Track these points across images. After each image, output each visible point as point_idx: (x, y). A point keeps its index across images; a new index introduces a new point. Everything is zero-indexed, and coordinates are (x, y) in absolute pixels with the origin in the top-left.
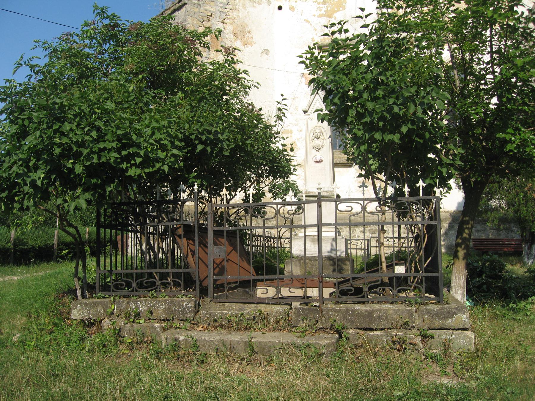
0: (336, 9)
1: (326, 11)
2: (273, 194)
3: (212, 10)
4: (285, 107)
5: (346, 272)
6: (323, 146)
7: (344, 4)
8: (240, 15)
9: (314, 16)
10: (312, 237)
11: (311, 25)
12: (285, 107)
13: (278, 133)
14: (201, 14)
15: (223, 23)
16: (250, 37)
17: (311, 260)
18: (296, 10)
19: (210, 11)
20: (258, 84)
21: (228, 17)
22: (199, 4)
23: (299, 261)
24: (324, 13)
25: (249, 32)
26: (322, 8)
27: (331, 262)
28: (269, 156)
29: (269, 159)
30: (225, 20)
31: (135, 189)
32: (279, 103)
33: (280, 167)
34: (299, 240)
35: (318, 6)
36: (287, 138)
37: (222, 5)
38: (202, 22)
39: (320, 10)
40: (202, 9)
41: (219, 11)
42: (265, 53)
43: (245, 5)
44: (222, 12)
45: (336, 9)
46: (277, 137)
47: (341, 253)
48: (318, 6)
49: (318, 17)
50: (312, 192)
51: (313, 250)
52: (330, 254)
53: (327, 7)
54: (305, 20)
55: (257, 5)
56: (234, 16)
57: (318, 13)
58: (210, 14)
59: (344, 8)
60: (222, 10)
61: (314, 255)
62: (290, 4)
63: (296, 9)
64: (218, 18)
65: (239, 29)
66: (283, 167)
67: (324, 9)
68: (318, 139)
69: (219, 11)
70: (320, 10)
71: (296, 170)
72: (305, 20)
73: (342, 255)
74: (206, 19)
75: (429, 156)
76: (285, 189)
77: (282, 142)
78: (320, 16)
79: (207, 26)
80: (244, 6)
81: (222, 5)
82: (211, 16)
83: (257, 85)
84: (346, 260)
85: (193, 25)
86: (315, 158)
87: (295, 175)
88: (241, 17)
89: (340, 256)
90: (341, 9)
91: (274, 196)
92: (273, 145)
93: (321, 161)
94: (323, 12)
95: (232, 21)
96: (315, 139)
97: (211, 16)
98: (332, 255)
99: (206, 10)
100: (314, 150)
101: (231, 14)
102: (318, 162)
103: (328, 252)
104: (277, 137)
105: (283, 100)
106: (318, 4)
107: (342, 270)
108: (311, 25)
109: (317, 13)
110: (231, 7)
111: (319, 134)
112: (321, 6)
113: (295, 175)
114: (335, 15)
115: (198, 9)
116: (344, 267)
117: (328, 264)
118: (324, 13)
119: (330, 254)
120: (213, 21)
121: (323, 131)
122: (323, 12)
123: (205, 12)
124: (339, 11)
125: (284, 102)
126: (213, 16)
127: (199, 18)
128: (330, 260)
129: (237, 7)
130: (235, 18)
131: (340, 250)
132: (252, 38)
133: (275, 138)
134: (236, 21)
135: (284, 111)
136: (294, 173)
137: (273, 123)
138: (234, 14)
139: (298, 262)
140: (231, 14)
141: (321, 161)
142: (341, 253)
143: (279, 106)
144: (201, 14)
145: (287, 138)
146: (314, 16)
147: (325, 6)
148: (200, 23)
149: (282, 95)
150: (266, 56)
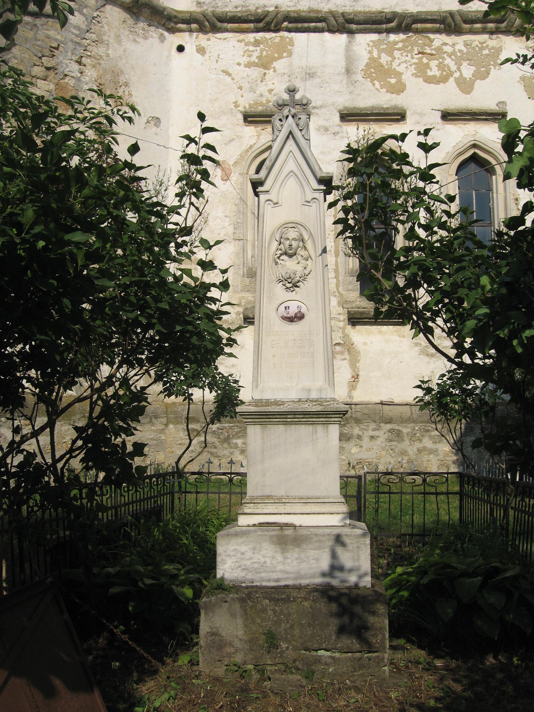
0: (276, 55)
1: (259, 58)
2: (165, 383)
3: (59, 37)
4: (210, 153)
5: (376, 635)
6: (304, 277)
7: (289, 47)
8: (110, 52)
9: (239, 64)
10: (274, 532)
11: (233, 79)
12: (210, 153)
13: (187, 231)
14: (39, 43)
15: (79, 63)
16: (127, 93)
17: (276, 601)
18: (208, 55)
19: (56, 40)
20: (133, 109)
21: (89, 54)
22: (35, 25)
23: (242, 600)
24: (256, 61)
25: (126, 84)
26: (253, 51)
27: (334, 607)
28: (157, 299)
29: (158, 309)
30: (83, 59)
31: (415, 254)
32: (191, 140)
33: (192, 334)
34: (240, 540)
35: (246, 48)
36: (218, 242)
37: (77, 32)
38: (40, 58)
39: (250, 56)
40: (41, 34)
41: (72, 41)
42: (152, 123)
43: (119, 36)
44: (78, 43)
45: (276, 55)
46: (185, 243)
47: (361, 577)
48: (246, 48)
49: (246, 66)
50: (276, 403)
51: (280, 567)
52: (327, 580)
53: (262, 51)
54: (223, 71)
55: (140, 40)
56: (100, 53)
57: (245, 60)
58: (55, 45)
59: (290, 54)
60: (78, 40)
61: (282, 583)
62: (198, 43)
63: (208, 52)
64: (70, 54)
65: (108, 77)
66: (200, 335)
67: (256, 54)
68: (291, 256)
69: (72, 41)
70: (250, 56)
71: (235, 341)
72: (223, 71)
73: (362, 584)
74: (47, 53)
75: (84, 306)
76: (190, 374)
77: (201, 254)
78: (249, 65)
79: (49, 65)
80: (118, 37)
81: (77, 32)
82: (57, 49)
83: (130, 114)
84: (377, 600)
85: (22, 61)
86: (282, 308)
87: (231, 355)
88: (111, 56)
89: (356, 586)
90: (285, 55)
91: (165, 390)
92: (172, 267)
93: (299, 317)
94: (254, 59)
95: (95, 61)
96: (284, 257)
97: (57, 49)
98: (335, 582)
99: (48, 37)
100: (279, 288)
101: (94, 50)
102: (290, 320)
103: (324, 575)
104: (185, 243)
105: (206, 130)
106: (246, 44)
107: (366, 628)
108: (233, 79)
109: (245, 60)
110: (94, 36)
111: (294, 244)
112: (251, 48)
113: (231, 355)
114: (275, 64)
115: (32, 33)
116: (372, 620)
117: (324, 610)
118: (256, 61)
119: (327, 580)
120: (61, 58)
121: (306, 237)
122: (254, 59)
123: (46, 40)
124: (280, 57)
125: (208, 138)
126: (61, 49)
127: (33, 50)
128: (331, 599)
129: (105, 38)
130: (101, 57)
131: (358, 569)
132: (130, 95)
133: (178, 246)
134: (102, 62)
135: (207, 164)
136: (227, 350)
137: (171, 200)
138: (101, 50)
139: (237, 606)
140: (94, 50)
141: (299, 317)
142: (361, 577)
143: (192, 149)
144: (39, 43)
145: (218, 242)
146: (239, 64)
147: (258, 49)
148: (35, 58)
149: (201, 117)
150: (154, 129)
